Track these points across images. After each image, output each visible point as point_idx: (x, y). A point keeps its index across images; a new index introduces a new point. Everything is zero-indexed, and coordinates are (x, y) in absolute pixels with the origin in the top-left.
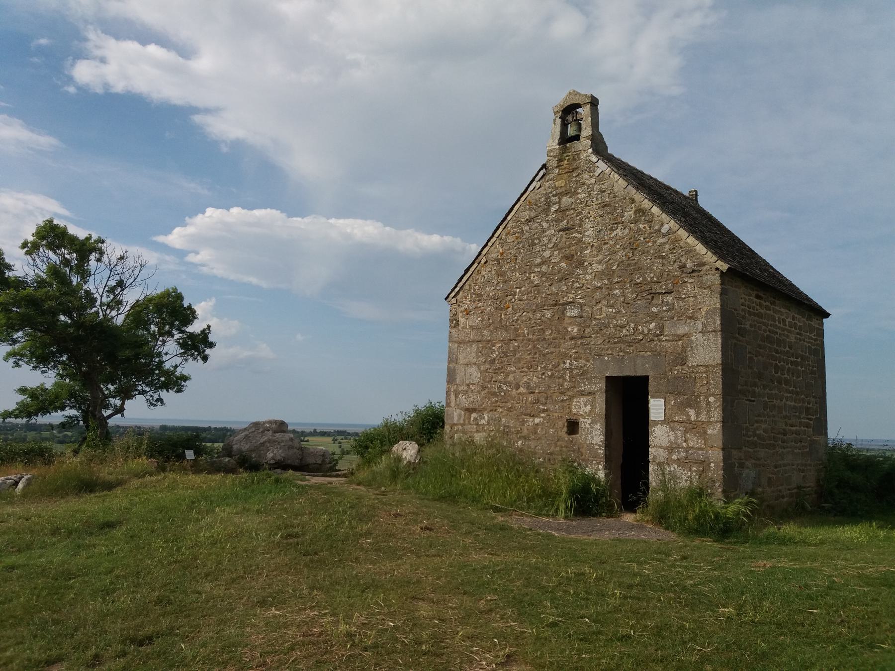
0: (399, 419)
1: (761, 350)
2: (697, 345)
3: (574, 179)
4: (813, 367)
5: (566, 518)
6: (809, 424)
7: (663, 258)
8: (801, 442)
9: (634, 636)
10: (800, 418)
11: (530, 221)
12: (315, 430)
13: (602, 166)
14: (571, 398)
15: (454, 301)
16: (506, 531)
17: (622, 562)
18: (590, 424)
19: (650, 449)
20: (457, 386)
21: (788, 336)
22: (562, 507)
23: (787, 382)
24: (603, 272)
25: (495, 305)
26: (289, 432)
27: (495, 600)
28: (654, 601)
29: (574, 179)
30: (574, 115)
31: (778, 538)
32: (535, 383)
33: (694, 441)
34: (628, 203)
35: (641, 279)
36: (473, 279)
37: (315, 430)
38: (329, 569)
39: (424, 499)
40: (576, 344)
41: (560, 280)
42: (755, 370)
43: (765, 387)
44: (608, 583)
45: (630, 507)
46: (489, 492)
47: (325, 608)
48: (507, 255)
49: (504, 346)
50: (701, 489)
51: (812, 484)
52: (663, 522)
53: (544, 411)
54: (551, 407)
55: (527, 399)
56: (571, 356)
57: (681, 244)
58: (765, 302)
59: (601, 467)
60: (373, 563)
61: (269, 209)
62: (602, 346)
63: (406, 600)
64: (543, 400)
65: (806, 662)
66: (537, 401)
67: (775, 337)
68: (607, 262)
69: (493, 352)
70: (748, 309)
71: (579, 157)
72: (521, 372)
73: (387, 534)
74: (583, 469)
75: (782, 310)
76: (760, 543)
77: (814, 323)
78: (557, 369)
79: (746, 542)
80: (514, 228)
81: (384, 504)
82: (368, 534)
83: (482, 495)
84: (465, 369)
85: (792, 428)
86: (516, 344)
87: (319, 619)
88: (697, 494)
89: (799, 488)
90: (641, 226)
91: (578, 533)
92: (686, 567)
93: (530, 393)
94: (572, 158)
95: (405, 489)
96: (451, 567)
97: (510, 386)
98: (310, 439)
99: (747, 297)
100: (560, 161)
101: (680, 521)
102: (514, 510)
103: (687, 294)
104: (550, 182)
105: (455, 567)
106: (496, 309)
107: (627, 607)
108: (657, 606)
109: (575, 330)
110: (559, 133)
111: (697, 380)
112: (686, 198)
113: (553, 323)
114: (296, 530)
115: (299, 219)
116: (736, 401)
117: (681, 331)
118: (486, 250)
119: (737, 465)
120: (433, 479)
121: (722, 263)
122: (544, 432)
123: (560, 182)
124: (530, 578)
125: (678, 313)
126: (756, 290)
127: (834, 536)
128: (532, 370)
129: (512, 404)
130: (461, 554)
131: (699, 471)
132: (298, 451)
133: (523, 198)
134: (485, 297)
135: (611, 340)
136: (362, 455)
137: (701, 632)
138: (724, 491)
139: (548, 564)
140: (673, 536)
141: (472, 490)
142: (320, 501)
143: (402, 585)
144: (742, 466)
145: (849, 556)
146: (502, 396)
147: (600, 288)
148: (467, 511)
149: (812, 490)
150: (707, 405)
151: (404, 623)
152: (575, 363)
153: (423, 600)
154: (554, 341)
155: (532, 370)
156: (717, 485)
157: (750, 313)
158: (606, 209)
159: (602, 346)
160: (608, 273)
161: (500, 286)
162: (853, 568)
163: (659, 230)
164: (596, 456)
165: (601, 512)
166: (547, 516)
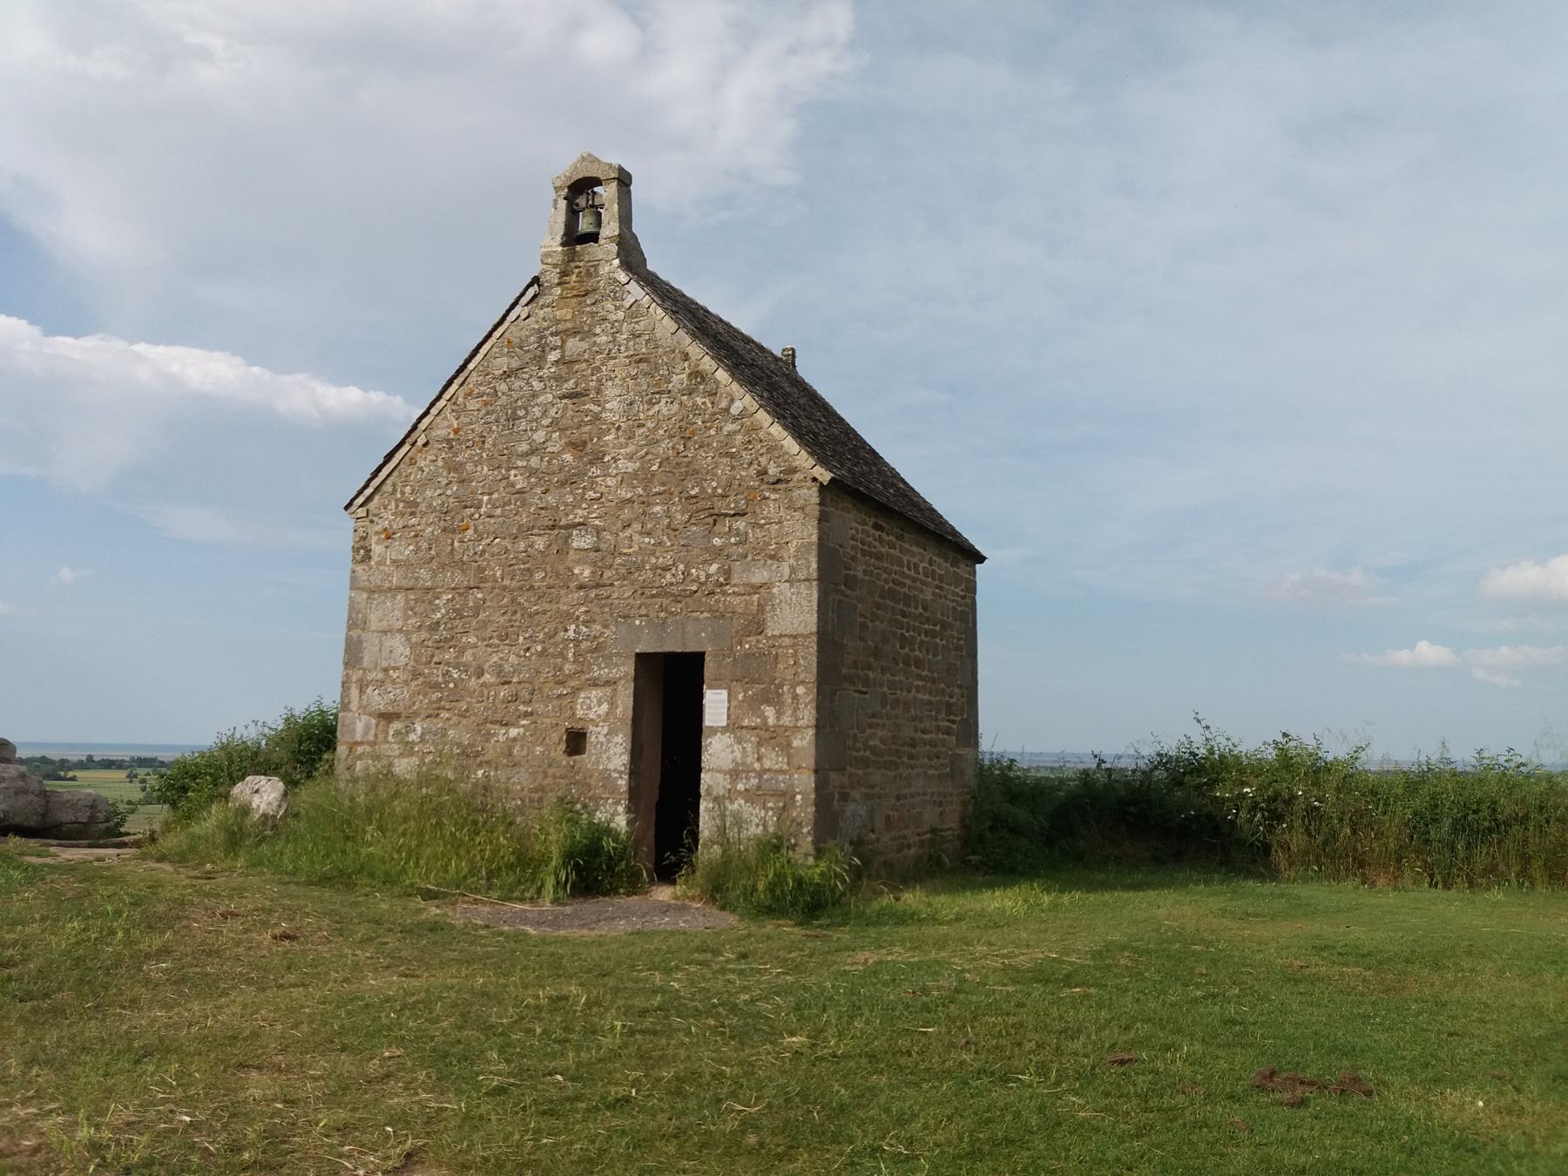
0: (251, 734)
1: (879, 612)
2: (781, 601)
3: (588, 309)
4: (959, 639)
5: (556, 901)
6: (951, 728)
7: (732, 456)
8: (938, 758)
9: (635, 1098)
10: (936, 720)
11: (509, 376)
12: (90, 758)
13: (636, 292)
14: (576, 691)
15: (362, 512)
16: (440, 932)
17: (637, 971)
18: (605, 736)
19: (703, 775)
20: (364, 672)
21: (921, 591)
22: (550, 883)
23: (919, 663)
24: (635, 475)
25: (442, 522)
26: (21, 761)
27: (399, 1056)
28: (681, 1035)
29: (588, 309)
30: (590, 197)
31: (894, 915)
32: (512, 666)
33: (773, 760)
34: (678, 360)
35: (697, 490)
36: (400, 474)
37: (90, 758)
38: (70, 1026)
39: (289, 883)
40: (587, 596)
41: (562, 484)
42: (870, 642)
43: (883, 671)
44: (606, 1009)
45: (666, 874)
46: (418, 863)
47: (53, 1099)
48: (466, 434)
49: (457, 598)
50: (779, 838)
51: (953, 825)
52: (718, 896)
53: (526, 715)
54: (539, 707)
55: (496, 695)
56: (578, 618)
57: (762, 434)
58: (888, 535)
59: (621, 809)
60: (167, 1006)
61: (24, 322)
62: (631, 601)
63: (225, 1071)
64: (525, 695)
65: (904, 1114)
66: (516, 698)
67: (902, 590)
68: (643, 457)
69: (437, 609)
70: (860, 546)
71: (596, 271)
72: (486, 646)
73: (203, 951)
74: (591, 814)
75: (914, 549)
76: (867, 925)
77: (962, 570)
78: (552, 641)
79: (844, 924)
80: (481, 385)
81: (207, 895)
82: (163, 953)
83: (404, 871)
84: (381, 641)
85: (925, 736)
86: (480, 596)
87: (37, 1120)
88: (774, 846)
89: (934, 831)
90: (699, 400)
91: (571, 927)
92: (741, 972)
93: (503, 684)
94: (584, 271)
95: (254, 865)
96: (324, 1003)
97: (467, 671)
98: (78, 774)
99: (860, 527)
100: (564, 274)
101: (745, 894)
102: (460, 894)
103: (767, 517)
104: (545, 310)
105: (330, 1003)
106: (444, 530)
107: (632, 1049)
108: (683, 1043)
109: (587, 573)
110: (563, 226)
111: (780, 659)
112: (776, 359)
113: (547, 560)
114: (10, 952)
115: (70, 340)
116: (838, 693)
118: (426, 421)
119: (836, 795)
120: (310, 846)
121: (822, 470)
122: (525, 752)
123: (564, 311)
124: (469, 1013)
125: (754, 548)
126: (877, 517)
127: (978, 907)
128: (507, 642)
129: (469, 703)
130: (346, 980)
131: (779, 808)
132: (36, 799)
133: (497, 334)
134: (423, 507)
135: (647, 591)
136: (174, 805)
137: (749, 1080)
138: (815, 842)
139: (505, 986)
140: (732, 919)
141: (384, 863)
142: (70, 894)
143: (219, 1044)
144: (844, 797)
145: (993, 939)
146: (450, 689)
147: (630, 501)
148: (371, 901)
149: (953, 835)
150: (793, 699)
151: (212, 1114)
152: (585, 630)
153: (259, 1068)
154: (549, 591)
155: (507, 642)
156: (805, 830)
157: (864, 553)
158: (643, 366)
159: (631, 601)
160: (644, 477)
161: (451, 489)
162: (997, 956)
163: (727, 410)
164: (614, 790)
165: (617, 887)
166: (522, 900)
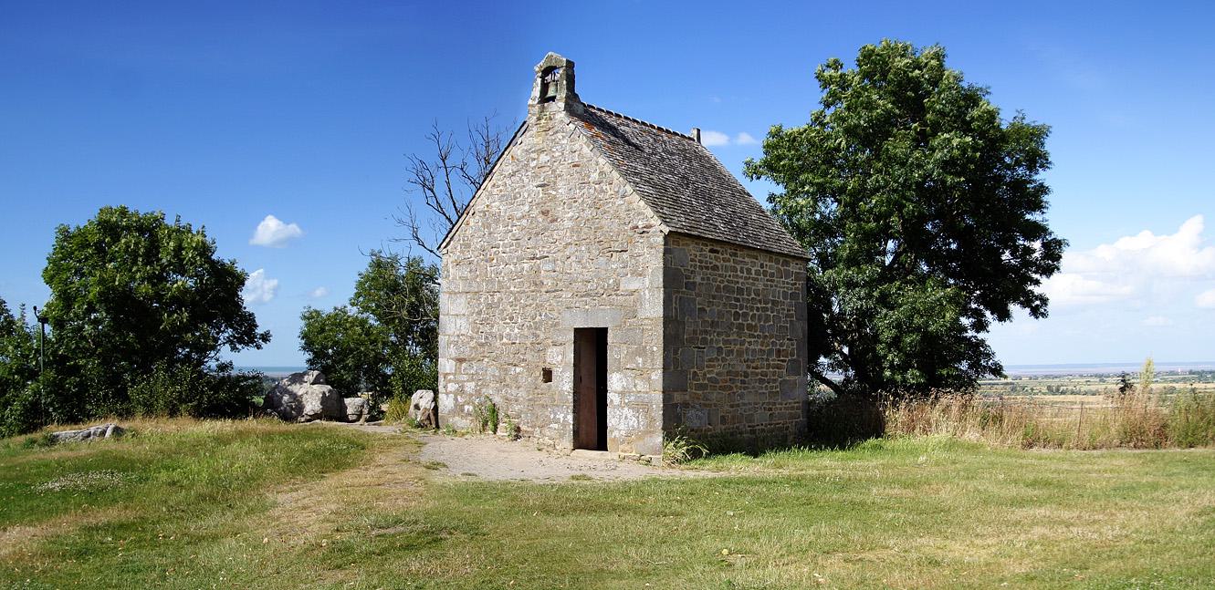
23: (750, 327)
33: (641, 386)
117: (632, 287)
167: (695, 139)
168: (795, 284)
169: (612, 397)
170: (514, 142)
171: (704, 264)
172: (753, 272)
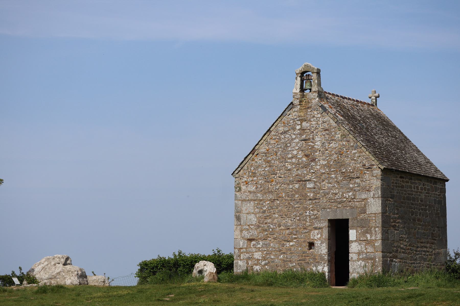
23: (419, 220)
33: (370, 249)
167: (374, 104)
168: (440, 195)
169: (352, 256)
170: (284, 114)
171: (397, 185)
172: (419, 188)
